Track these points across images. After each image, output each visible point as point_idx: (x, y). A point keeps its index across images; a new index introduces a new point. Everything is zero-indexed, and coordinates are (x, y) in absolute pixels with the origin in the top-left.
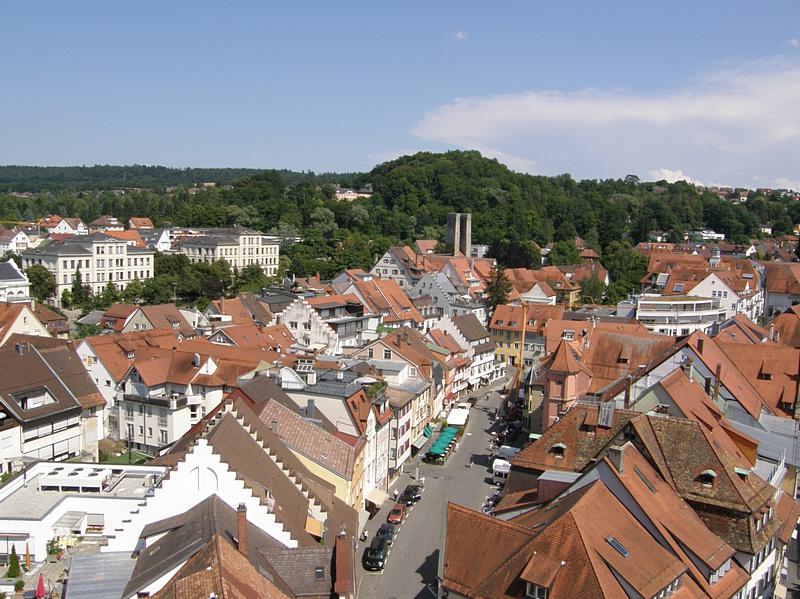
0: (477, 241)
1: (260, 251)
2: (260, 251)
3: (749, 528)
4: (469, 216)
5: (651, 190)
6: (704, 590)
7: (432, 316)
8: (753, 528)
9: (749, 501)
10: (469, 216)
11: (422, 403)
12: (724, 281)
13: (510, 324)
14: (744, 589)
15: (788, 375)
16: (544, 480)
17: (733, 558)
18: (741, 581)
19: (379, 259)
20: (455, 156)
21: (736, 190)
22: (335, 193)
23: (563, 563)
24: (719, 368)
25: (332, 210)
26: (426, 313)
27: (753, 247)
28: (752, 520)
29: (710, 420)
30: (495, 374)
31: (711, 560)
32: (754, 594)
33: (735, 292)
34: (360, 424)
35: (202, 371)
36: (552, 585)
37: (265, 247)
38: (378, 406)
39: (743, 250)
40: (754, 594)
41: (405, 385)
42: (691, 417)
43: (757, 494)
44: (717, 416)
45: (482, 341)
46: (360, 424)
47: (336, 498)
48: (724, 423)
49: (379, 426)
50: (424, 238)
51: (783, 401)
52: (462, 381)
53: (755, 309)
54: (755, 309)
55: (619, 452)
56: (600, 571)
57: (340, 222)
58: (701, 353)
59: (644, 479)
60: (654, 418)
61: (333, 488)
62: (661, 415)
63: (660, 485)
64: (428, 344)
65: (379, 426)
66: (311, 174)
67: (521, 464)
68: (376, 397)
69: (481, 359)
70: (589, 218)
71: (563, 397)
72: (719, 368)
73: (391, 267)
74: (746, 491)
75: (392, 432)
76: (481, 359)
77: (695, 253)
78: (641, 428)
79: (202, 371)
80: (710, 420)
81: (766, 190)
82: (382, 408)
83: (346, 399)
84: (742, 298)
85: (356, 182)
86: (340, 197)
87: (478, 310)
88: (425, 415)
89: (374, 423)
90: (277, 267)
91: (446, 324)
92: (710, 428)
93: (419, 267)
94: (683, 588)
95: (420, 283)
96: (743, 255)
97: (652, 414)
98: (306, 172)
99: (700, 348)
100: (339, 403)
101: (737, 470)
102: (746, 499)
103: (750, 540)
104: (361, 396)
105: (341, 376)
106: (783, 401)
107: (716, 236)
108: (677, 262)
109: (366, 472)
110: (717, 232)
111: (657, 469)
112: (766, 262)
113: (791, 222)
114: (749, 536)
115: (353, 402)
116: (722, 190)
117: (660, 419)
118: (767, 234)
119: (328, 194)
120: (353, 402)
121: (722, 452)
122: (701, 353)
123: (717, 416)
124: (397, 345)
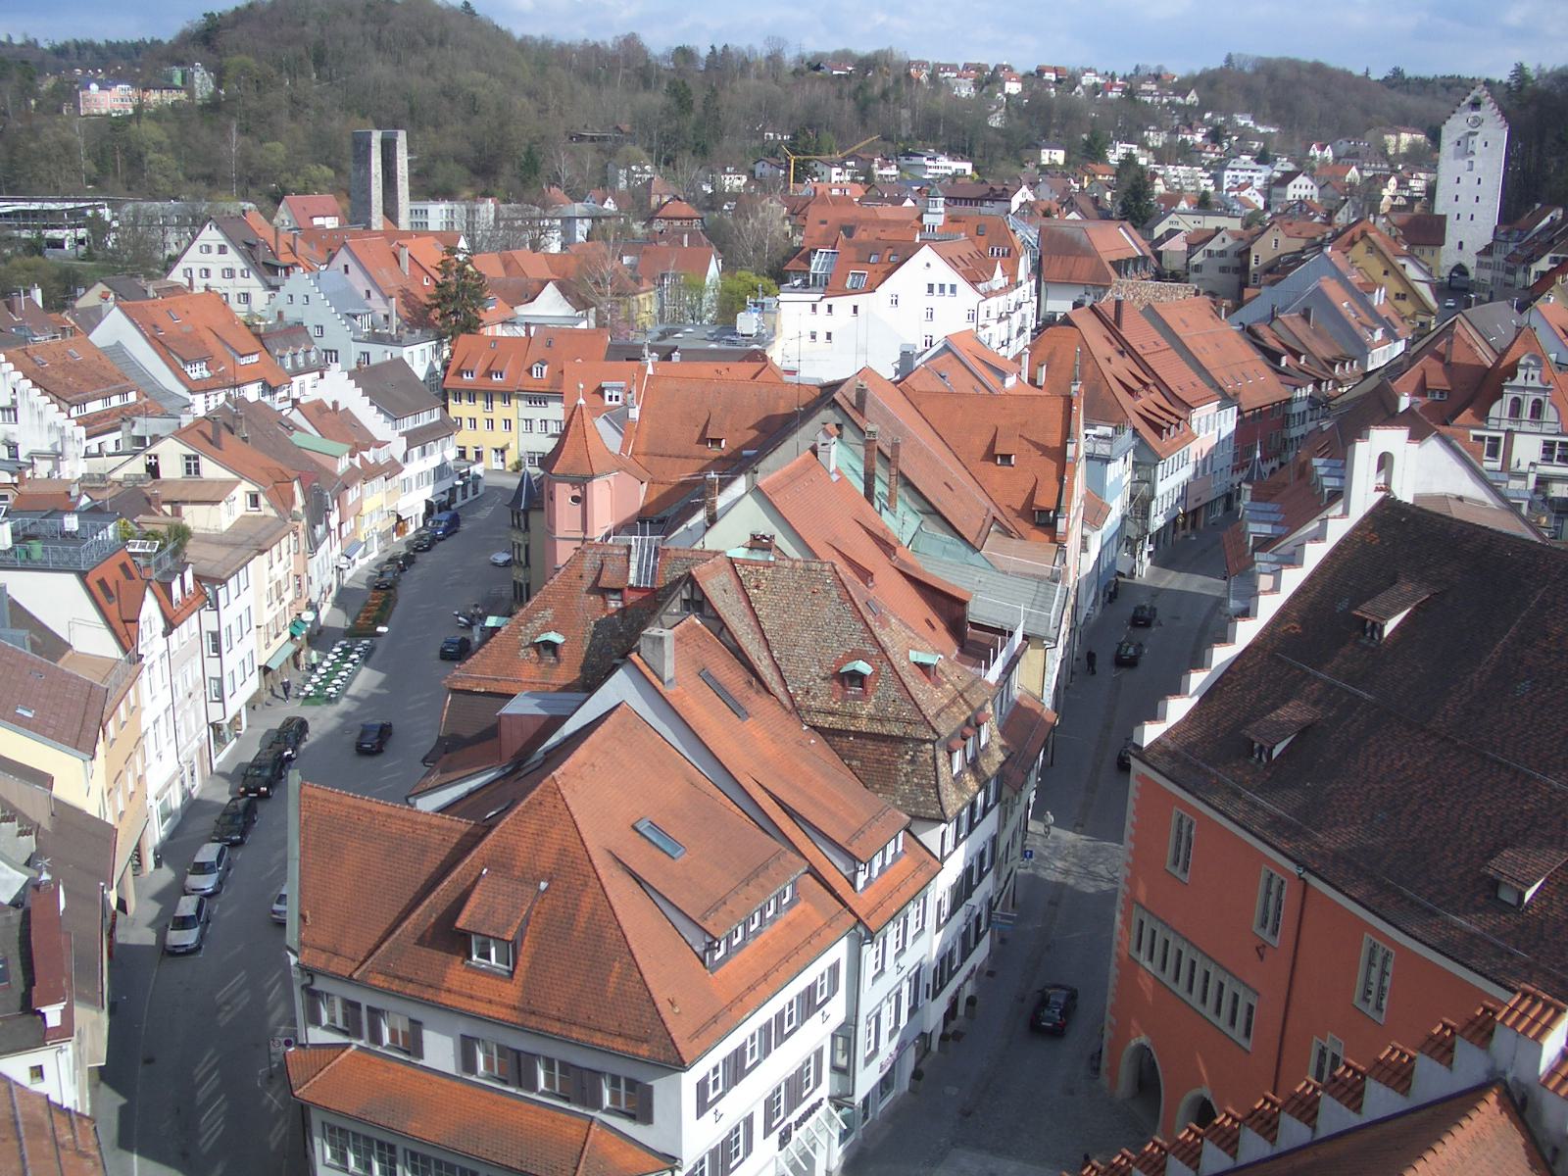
3: (936, 769)
4: (402, 137)
6: (844, 904)
7: (308, 370)
8: (943, 769)
9: (938, 715)
10: (402, 137)
11: (279, 572)
12: (951, 262)
13: (489, 373)
14: (930, 890)
15: (1037, 445)
16: (509, 716)
17: (907, 830)
18: (922, 877)
23: (543, 885)
26: (294, 362)
27: (1024, 189)
28: (942, 756)
29: (868, 554)
32: (981, 865)
33: (973, 283)
34: (124, 629)
36: (522, 932)
38: (167, 588)
39: (1004, 196)
40: (981, 865)
41: (235, 529)
42: (827, 555)
46: (124, 629)
47: (56, 800)
48: (903, 562)
49: (170, 626)
55: (661, 639)
56: (620, 891)
60: (745, 562)
61: (45, 780)
62: (758, 556)
63: (758, 703)
64: (296, 438)
65: (170, 626)
67: (467, 686)
71: (586, 532)
73: (217, 262)
75: (208, 644)
77: (908, 203)
78: (717, 587)
80: (868, 554)
82: (176, 586)
83: (82, 576)
84: (988, 295)
87: (417, 349)
88: (289, 596)
89: (159, 624)
91: (337, 388)
92: (865, 575)
93: (286, 259)
94: (800, 906)
95: (284, 292)
96: (1005, 205)
97: (740, 553)
98: (18, 40)
100: (71, 581)
101: (914, 656)
102: (930, 712)
103: (938, 793)
105: (71, 523)
108: (861, 222)
109: (150, 739)
111: (753, 671)
112: (1045, 222)
114: (937, 786)
115: (102, 583)
117: (757, 563)
118: (1053, 165)
120: (102, 583)
121: (885, 623)
123: (886, 546)
124: (214, 442)
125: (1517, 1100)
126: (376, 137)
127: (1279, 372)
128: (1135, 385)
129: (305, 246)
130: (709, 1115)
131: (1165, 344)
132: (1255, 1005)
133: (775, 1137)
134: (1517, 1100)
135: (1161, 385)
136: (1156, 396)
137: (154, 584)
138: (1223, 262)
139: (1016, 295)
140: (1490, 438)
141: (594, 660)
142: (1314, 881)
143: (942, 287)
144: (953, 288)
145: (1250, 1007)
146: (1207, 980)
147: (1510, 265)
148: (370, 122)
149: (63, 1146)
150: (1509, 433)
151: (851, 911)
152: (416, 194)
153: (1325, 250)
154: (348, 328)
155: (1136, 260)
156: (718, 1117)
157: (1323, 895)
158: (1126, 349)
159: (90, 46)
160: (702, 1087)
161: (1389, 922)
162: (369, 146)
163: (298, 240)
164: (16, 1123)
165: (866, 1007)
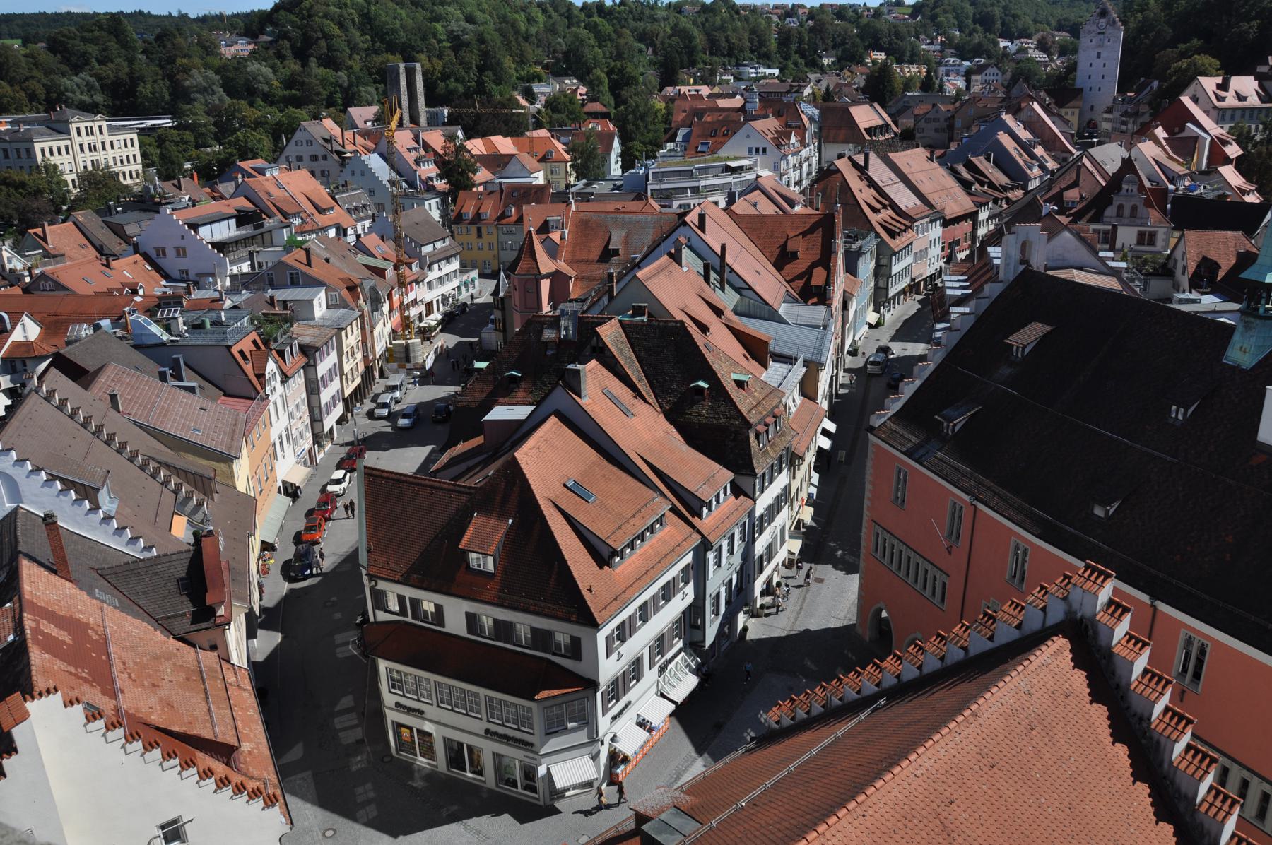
0: (433, 99)
1: (108, 146)
2: (108, 146)
5: (680, 12)
15: (786, 242)
19: (288, 141)
20: (40, 13)
21: (793, 5)
22: (218, 46)
24: (723, 247)
25: (217, 73)
30: (463, 289)
31: (704, 493)
35: (17, 336)
37: (114, 138)
43: (759, 403)
44: (718, 312)
45: (439, 245)
50: (1100, 143)
51: (611, 247)
52: (415, 302)
53: (805, 166)
54: (805, 166)
57: (231, 90)
58: (703, 231)
59: (615, 401)
66: (184, 17)
68: (276, 340)
69: (440, 269)
70: (594, 59)
72: (723, 247)
74: (743, 402)
76: (440, 269)
79: (17, 336)
80: (706, 316)
81: (832, 5)
85: (251, 25)
86: (228, 52)
90: (139, 167)
92: (704, 328)
94: (667, 529)
99: (702, 226)
101: (734, 376)
104: (254, 342)
106: (611, 247)
107: (768, 71)
110: (769, 67)
113: (861, 50)
116: (776, 7)
119: (209, 49)
120: (241, 352)
122: (703, 231)
123: (718, 312)
125: (727, 287)
126: (402, 66)
127: (970, 194)
128: (878, 206)
129: (362, 139)
130: (614, 656)
131: (896, 179)
132: (947, 582)
133: (656, 668)
134: (727, 287)
135: (894, 206)
136: (890, 212)
137: (274, 352)
138: (937, 125)
139: (805, 153)
140: (1143, 244)
141: (573, 618)
142: (981, 506)
143: (757, 150)
144: (764, 150)
145: (944, 584)
146: (909, 561)
147: (1124, 119)
148: (398, 56)
149: (230, 684)
150: (1115, 227)
151: (699, 532)
152: (429, 103)
153: (20, 41)
154: (73, 494)
155: (881, 127)
156: (620, 656)
157: (986, 514)
158: (872, 184)
159: (220, 17)
160: (609, 640)
161: (1027, 530)
162: (398, 74)
163: (357, 136)
164: (201, 672)
165: (711, 589)
